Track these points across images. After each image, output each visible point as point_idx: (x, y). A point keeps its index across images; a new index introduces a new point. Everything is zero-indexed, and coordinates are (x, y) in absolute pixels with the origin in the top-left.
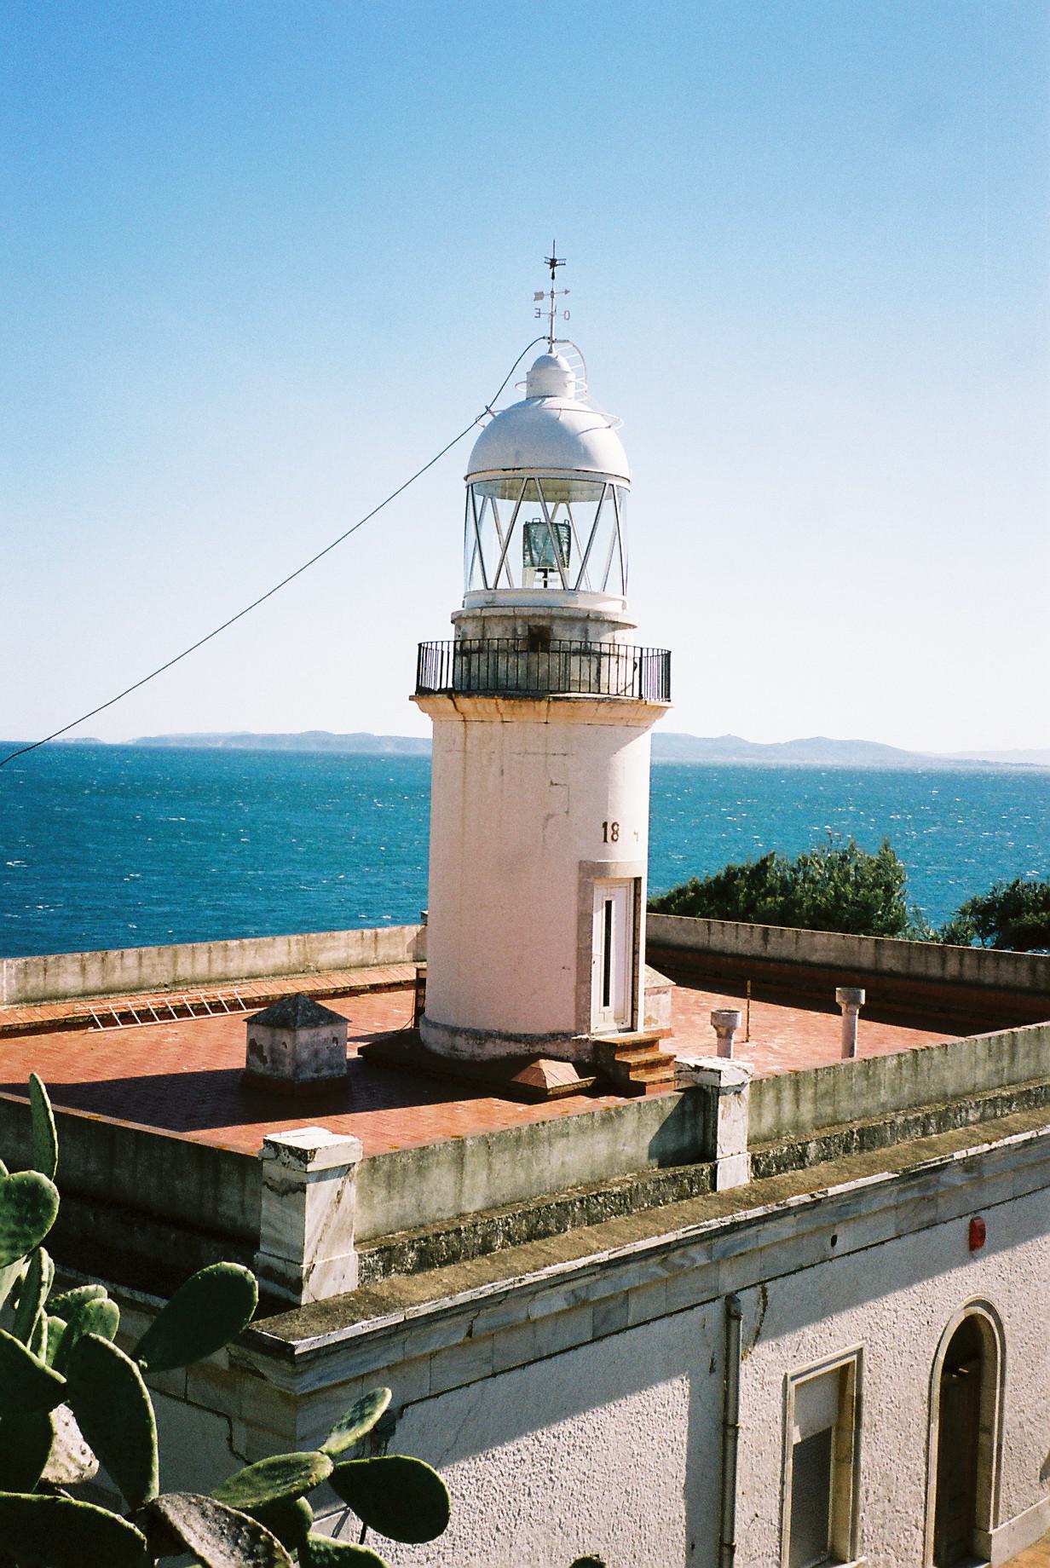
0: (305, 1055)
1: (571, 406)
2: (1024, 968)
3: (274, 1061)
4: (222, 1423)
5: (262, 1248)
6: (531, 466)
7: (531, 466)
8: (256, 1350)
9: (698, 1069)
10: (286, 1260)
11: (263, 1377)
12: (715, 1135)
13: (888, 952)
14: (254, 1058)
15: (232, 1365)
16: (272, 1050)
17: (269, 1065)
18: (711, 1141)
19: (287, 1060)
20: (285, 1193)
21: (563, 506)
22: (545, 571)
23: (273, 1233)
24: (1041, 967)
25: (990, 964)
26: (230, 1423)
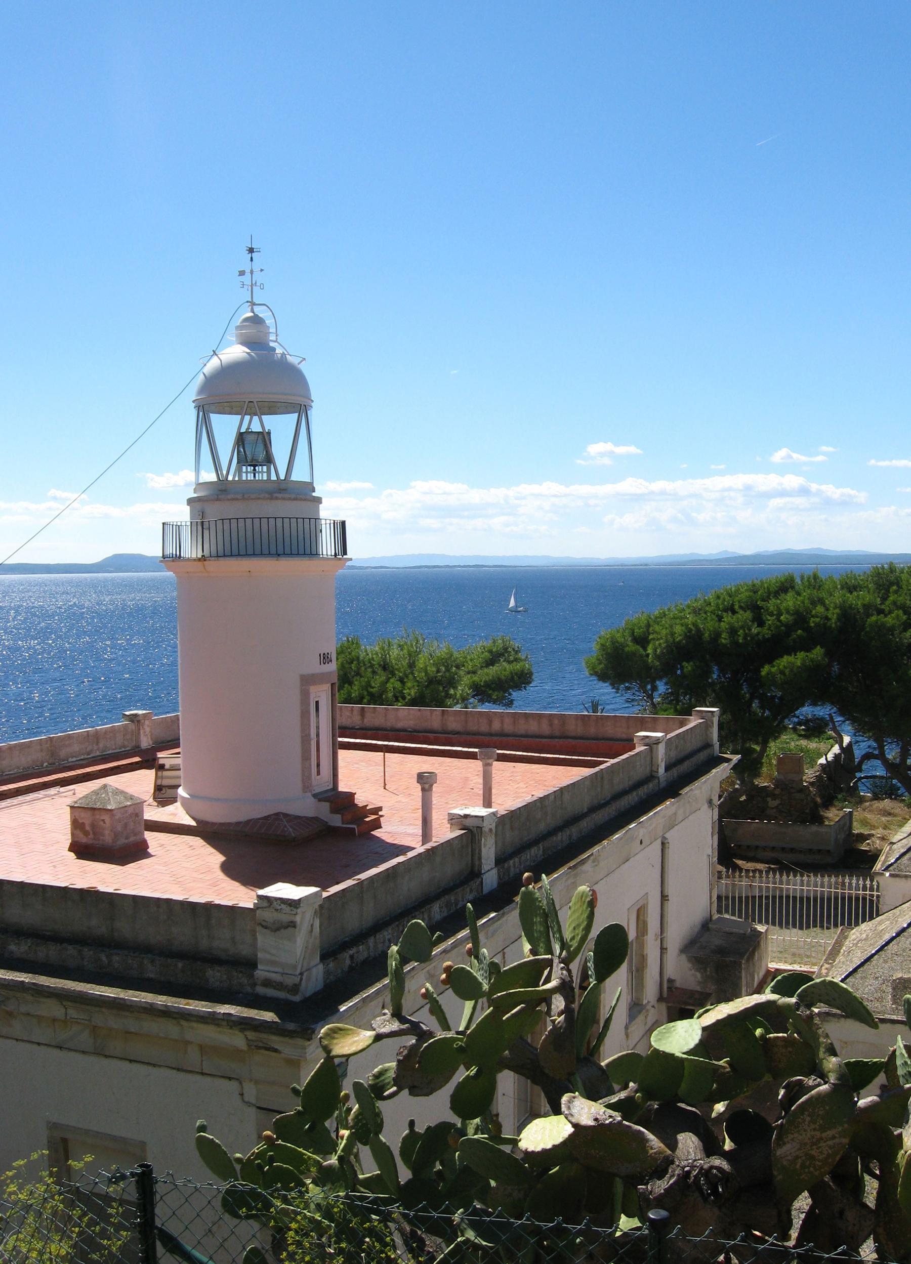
0: (119, 828)
1: (287, 343)
2: (507, 721)
3: (94, 833)
4: (234, 1084)
5: (259, 967)
6: (256, 389)
7: (256, 389)
8: (274, 1034)
9: (466, 816)
10: (282, 974)
11: (276, 1051)
12: (480, 858)
13: (452, 718)
14: (78, 832)
15: (249, 1046)
16: (93, 826)
17: (91, 836)
18: (477, 863)
19: (107, 832)
20: (278, 929)
21: (256, 418)
22: (254, 466)
23: (268, 957)
24: (556, 722)
25: (522, 721)
26: (241, 1083)
